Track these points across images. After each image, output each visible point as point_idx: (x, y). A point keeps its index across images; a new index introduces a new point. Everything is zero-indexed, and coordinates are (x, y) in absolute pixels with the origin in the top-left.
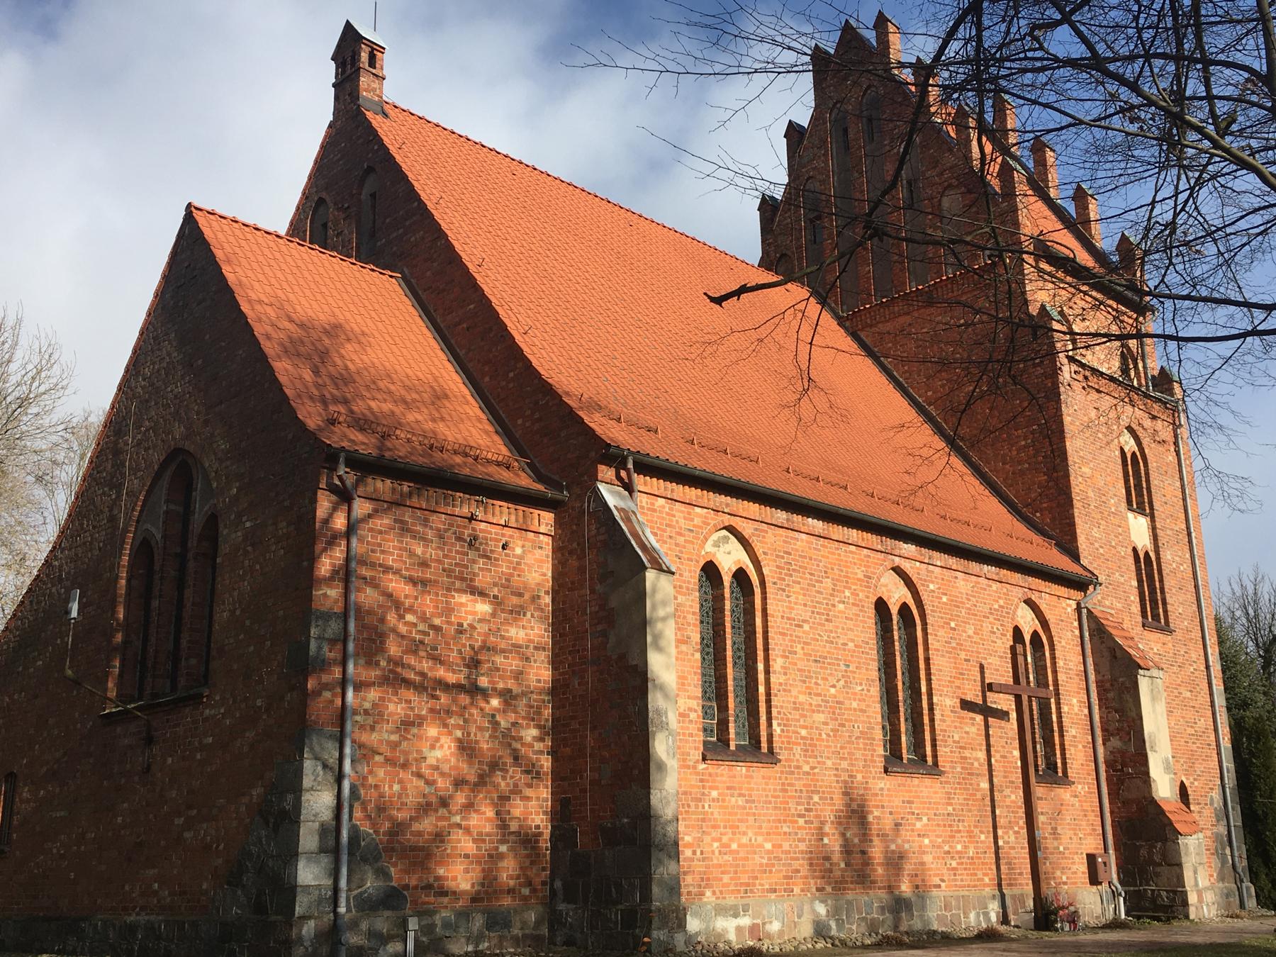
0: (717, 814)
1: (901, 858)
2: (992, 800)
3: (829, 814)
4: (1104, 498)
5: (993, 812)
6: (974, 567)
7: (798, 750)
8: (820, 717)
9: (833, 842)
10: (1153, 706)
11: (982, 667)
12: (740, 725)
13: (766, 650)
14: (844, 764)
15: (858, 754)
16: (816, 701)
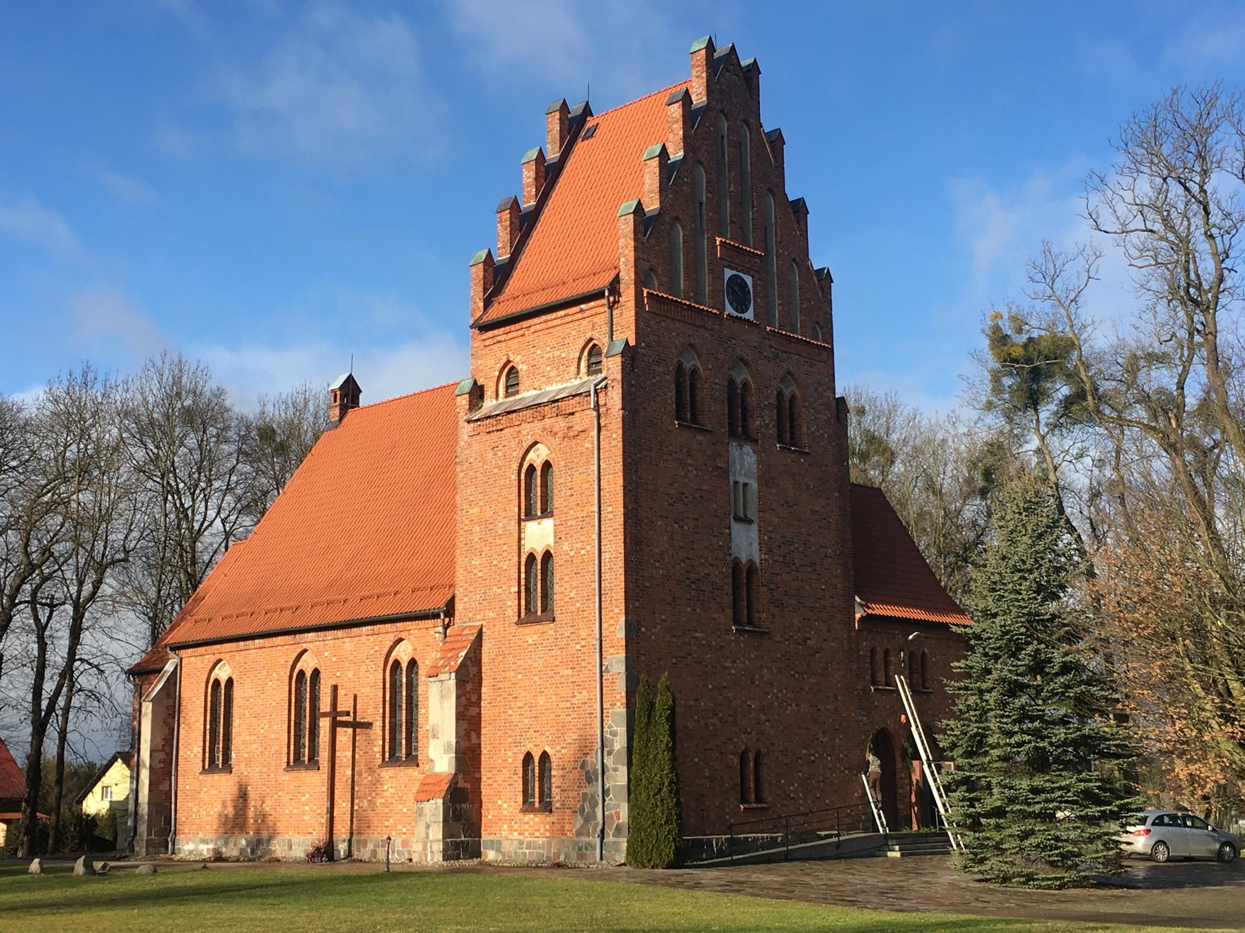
0: (206, 798)
1: (551, 811)
2: (353, 781)
3: (229, 798)
4: (491, 527)
5: (353, 788)
6: (355, 631)
7: (243, 765)
8: (255, 746)
9: (230, 811)
10: (441, 704)
11: (355, 697)
12: (219, 756)
13: (384, 688)
14: (265, 769)
15: (273, 763)
16: (253, 738)
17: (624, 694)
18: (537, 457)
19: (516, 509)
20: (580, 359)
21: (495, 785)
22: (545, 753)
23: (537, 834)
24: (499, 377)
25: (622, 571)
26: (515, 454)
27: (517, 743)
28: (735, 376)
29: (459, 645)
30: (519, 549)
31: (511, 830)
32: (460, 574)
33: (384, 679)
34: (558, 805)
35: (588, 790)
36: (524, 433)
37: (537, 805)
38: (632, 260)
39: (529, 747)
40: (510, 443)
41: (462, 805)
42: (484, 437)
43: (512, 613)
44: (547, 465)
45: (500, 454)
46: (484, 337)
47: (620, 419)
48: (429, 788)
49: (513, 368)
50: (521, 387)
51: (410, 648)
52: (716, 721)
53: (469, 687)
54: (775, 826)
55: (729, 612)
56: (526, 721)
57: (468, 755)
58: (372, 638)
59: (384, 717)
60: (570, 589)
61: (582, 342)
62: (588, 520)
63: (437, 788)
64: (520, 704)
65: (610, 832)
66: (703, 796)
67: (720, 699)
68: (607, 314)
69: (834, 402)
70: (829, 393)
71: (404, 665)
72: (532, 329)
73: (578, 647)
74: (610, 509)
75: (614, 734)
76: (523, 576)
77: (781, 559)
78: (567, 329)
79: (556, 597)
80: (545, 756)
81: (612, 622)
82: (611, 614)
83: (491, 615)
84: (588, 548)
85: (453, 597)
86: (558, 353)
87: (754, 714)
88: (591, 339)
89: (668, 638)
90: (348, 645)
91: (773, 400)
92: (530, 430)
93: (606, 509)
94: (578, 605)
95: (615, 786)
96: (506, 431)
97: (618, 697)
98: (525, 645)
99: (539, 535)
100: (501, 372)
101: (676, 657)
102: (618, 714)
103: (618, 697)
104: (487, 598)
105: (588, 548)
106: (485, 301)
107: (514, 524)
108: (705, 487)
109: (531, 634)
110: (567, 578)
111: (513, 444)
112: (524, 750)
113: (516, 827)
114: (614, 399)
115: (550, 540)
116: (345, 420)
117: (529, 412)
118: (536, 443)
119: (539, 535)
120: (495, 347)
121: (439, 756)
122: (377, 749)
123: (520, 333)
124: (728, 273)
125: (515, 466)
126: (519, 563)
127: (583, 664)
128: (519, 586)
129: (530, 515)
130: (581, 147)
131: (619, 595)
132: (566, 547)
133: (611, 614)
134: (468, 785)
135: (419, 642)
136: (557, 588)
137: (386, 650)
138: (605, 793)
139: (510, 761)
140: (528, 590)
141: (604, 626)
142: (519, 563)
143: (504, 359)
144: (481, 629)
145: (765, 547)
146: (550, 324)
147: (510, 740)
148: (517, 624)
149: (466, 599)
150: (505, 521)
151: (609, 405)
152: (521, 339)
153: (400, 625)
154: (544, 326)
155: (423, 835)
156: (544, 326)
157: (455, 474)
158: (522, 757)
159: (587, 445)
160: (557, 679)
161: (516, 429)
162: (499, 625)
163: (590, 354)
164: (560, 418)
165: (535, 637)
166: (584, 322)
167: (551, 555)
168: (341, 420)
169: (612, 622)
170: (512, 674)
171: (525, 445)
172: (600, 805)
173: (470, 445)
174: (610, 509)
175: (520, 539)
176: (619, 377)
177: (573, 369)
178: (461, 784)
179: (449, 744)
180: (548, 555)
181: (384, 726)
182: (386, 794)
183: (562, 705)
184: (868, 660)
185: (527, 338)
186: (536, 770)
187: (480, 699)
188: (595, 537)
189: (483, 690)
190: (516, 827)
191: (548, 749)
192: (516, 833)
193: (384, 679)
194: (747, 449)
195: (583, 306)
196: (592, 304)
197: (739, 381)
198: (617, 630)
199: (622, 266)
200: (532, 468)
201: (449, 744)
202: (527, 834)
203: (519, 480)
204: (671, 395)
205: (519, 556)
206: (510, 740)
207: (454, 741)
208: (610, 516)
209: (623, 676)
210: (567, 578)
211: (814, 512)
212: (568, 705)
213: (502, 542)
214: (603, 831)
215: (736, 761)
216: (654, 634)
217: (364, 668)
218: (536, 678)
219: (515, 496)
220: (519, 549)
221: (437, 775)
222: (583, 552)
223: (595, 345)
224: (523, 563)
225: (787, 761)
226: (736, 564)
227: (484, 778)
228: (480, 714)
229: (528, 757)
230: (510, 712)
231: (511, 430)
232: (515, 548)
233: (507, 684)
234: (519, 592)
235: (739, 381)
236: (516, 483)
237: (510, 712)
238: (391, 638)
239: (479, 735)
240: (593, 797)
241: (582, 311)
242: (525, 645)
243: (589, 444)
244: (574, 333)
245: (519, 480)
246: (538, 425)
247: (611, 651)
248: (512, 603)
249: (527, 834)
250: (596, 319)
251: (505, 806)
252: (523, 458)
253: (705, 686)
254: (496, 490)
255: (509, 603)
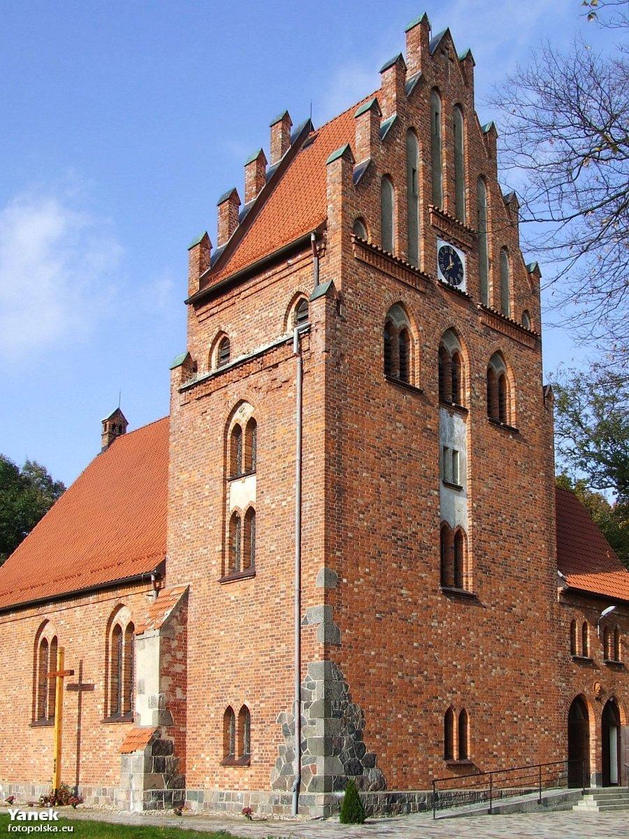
4: (198, 490)
6: (84, 600)
17: (322, 645)
18: (241, 418)
19: (222, 470)
20: (286, 316)
21: (199, 739)
22: (244, 707)
23: (236, 786)
24: (212, 349)
25: (322, 518)
26: (221, 415)
27: (220, 699)
28: (446, 345)
29: (167, 605)
30: (224, 508)
31: (213, 782)
32: (171, 538)
33: (107, 642)
34: (256, 758)
35: (286, 743)
36: (230, 393)
37: (237, 758)
38: (339, 205)
39: (230, 701)
40: (217, 405)
41: (165, 760)
42: (194, 404)
43: (216, 572)
44: (252, 423)
45: (208, 418)
46: (198, 313)
47: (323, 362)
48: (135, 740)
49: (225, 339)
50: (232, 354)
51: (129, 614)
52: (420, 678)
53: (175, 644)
54: (478, 783)
55: (437, 573)
56: (227, 677)
57: (173, 711)
58: (97, 606)
59: (106, 677)
60: (268, 542)
61: (288, 298)
62: (289, 470)
63: (140, 741)
64: (222, 660)
65: (306, 785)
66: (406, 752)
67: (426, 658)
68: (314, 266)
69: (541, 389)
70: (536, 379)
71: (124, 629)
72: (242, 296)
73: (278, 600)
74: (311, 456)
75: (312, 686)
76: (227, 535)
77: (489, 527)
78: (275, 289)
79: (257, 552)
80: (245, 710)
81: (311, 572)
82: (311, 564)
83: (198, 575)
84: (289, 499)
85: (164, 561)
86: (266, 314)
87: (459, 674)
88: (299, 293)
89: (372, 592)
90: (79, 613)
91: (484, 374)
92: (236, 390)
93: (308, 456)
94: (278, 558)
95: (311, 740)
96: (214, 394)
97: (317, 648)
98: (228, 602)
99: (243, 494)
100: (214, 344)
101: (380, 612)
102: (316, 666)
103: (317, 648)
104: (193, 554)
105: (289, 499)
106: (201, 280)
107: (219, 487)
108: (413, 446)
109: (234, 591)
110: (268, 532)
111: (220, 407)
112: (225, 705)
113: (217, 779)
114: (318, 342)
115: (253, 498)
116: (112, 445)
117: (235, 373)
118: (241, 402)
119: (243, 494)
120: (208, 321)
121: (146, 714)
122: (100, 707)
123: (231, 301)
124: (442, 244)
125: (221, 428)
126: (224, 522)
127: (282, 617)
128: (223, 544)
129: (235, 477)
130: (303, 156)
131: (319, 543)
132: (267, 501)
133: (311, 564)
134: (172, 739)
135: (137, 606)
136: (258, 543)
137: (108, 616)
138: (302, 746)
139: (212, 715)
140: (232, 548)
141: (304, 576)
142: (224, 522)
143: (217, 330)
144: (188, 590)
145: (476, 514)
146: (259, 287)
147: (212, 695)
148: (220, 581)
149: (175, 562)
150: (212, 482)
151: (312, 350)
152: (232, 308)
153: (120, 592)
154: (253, 290)
155: (127, 785)
156: (253, 290)
157: (167, 445)
158: (223, 711)
159: (290, 395)
160: (258, 634)
161: (224, 390)
162: (204, 584)
163: (297, 309)
164: (264, 372)
165: (237, 594)
166: (291, 278)
167: (254, 512)
168: (109, 445)
169: (311, 572)
170: (215, 631)
171: (231, 405)
172: (297, 759)
173: (181, 414)
174: (311, 456)
175: (225, 499)
176: (323, 319)
177: (280, 326)
178: (164, 737)
179: (153, 699)
180: (251, 512)
181: (106, 686)
182: (108, 747)
183: (262, 659)
184: (567, 631)
185: (237, 306)
186: (238, 722)
187: (185, 656)
188: (296, 486)
189: (190, 648)
190: (217, 779)
191: (247, 704)
192: (217, 786)
193: (107, 642)
194: (457, 419)
195: (290, 262)
196: (300, 257)
197: (450, 351)
198: (316, 581)
199: (329, 213)
200: (238, 428)
201: (141, 692)
202: (227, 786)
203: (226, 441)
204: (379, 349)
205: (224, 515)
206: (212, 695)
207: (157, 696)
208: (312, 463)
209: (321, 628)
210: (268, 532)
211: (520, 487)
212: (267, 659)
213: (208, 503)
214: (299, 784)
215: (441, 718)
216: (358, 586)
217: (90, 633)
218: (237, 634)
219: (221, 457)
220: (224, 508)
221: (144, 728)
222: (284, 503)
223: (302, 300)
224: (227, 523)
225: (491, 720)
226: (445, 528)
227: (189, 733)
228: (185, 671)
229: (229, 711)
230: (213, 668)
231: (219, 392)
232: (220, 507)
233: (210, 642)
234: (223, 551)
235: (450, 351)
236: (222, 444)
237: (213, 668)
238: (112, 604)
239: (185, 691)
240: (290, 751)
241: (290, 266)
242: (228, 602)
243: (292, 393)
244: (281, 290)
245: (226, 441)
246: (244, 384)
247: (311, 601)
248: (216, 561)
249: (227, 786)
250: (303, 272)
251: (208, 759)
252: (229, 419)
253: (410, 643)
254: (204, 454)
255: (214, 563)
